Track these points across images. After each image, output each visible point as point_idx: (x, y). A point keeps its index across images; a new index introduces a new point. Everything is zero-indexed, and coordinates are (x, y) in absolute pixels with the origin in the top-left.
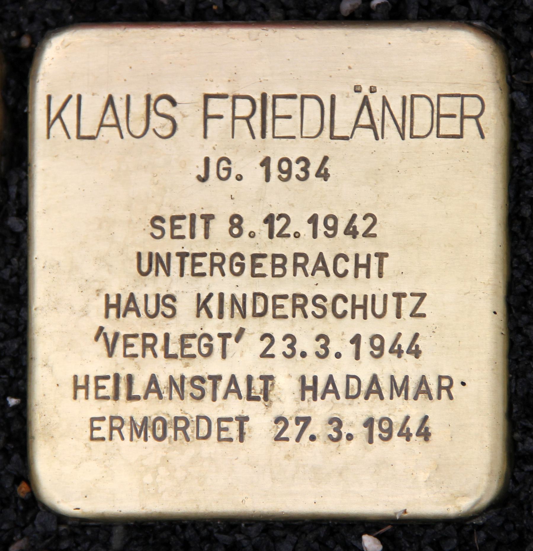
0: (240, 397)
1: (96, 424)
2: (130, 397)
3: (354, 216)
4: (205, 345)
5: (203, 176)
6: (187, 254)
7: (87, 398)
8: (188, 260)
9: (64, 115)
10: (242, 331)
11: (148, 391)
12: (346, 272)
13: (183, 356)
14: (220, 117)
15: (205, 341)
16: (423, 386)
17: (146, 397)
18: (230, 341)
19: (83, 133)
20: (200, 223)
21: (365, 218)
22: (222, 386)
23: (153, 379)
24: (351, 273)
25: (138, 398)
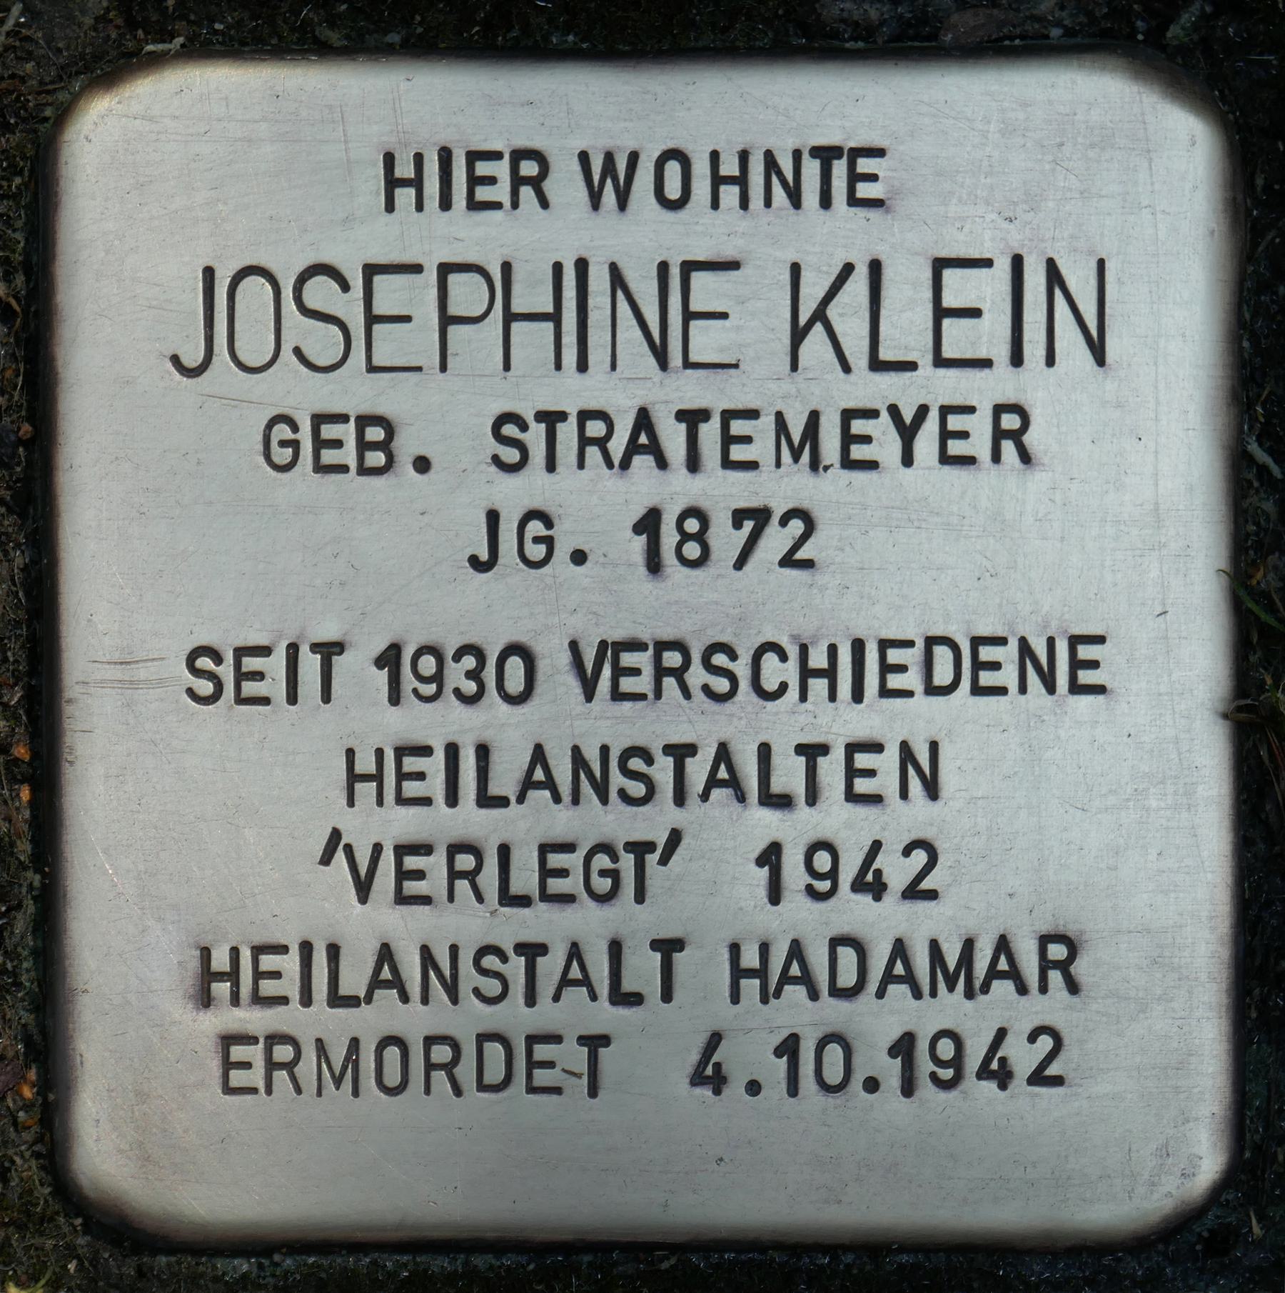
1: (555, 860)
4: (603, 873)
5: (484, 556)
9: (832, 312)
10: (675, 838)
12: (783, 687)
13: (546, 897)
14: (975, 313)
15: (602, 861)
16: (1003, 958)
17: (521, 799)
18: (652, 859)
19: (947, 353)
20: (310, 664)
23: (386, 954)
24: (793, 693)
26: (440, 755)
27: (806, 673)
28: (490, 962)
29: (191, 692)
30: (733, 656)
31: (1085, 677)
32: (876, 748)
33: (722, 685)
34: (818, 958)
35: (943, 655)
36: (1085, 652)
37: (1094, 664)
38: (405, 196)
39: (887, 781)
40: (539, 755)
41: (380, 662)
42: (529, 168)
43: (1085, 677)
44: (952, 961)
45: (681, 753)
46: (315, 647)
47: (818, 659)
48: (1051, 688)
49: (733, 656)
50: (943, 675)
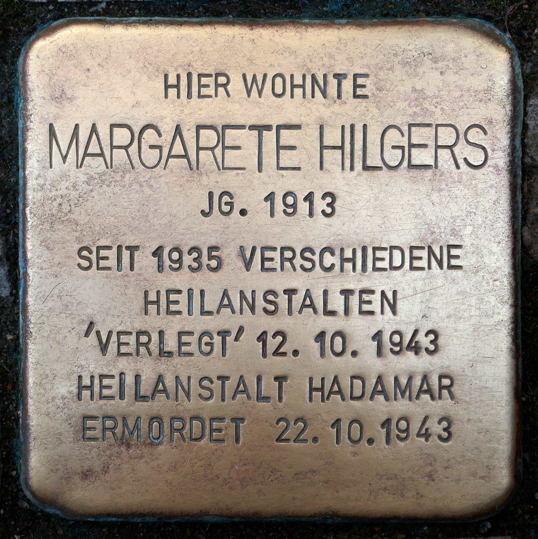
0: (315, 311)
1: (185, 339)
2: (203, 312)
3: (416, 332)
5: (207, 210)
6: (268, 128)
7: (158, 313)
8: (269, 137)
10: (241, 330)
11: (221, 306)
13: (180, 353)
16: (242, 385)
17: (218, 312)
18: (230, 339)
20: (126, 254)
21: (427, 335)
22: (298, 299)
24: (337, 268)
25: (210, 313)
26: (185, 294)
27: (344, 260)
28: (206, 383)
29: (79, 265)
30: (313, 253)
31: (454, 262)
32: (372, 292)
33: (308, 265)
34: (345, 383)
35: (397, 254)
36: (454, 252)
37: (457, 257)
38: (172, 92)
39: (376, 306)
40: (225, 294)
41: (154, 254)
42: (222, 80)
43: (454, 262)
44: (131, 426)
45: (290, 292)
46: (128, 248)
47: (348, 254)
48: (441, 267)
49: (313, 253)
50: (397, 262)
